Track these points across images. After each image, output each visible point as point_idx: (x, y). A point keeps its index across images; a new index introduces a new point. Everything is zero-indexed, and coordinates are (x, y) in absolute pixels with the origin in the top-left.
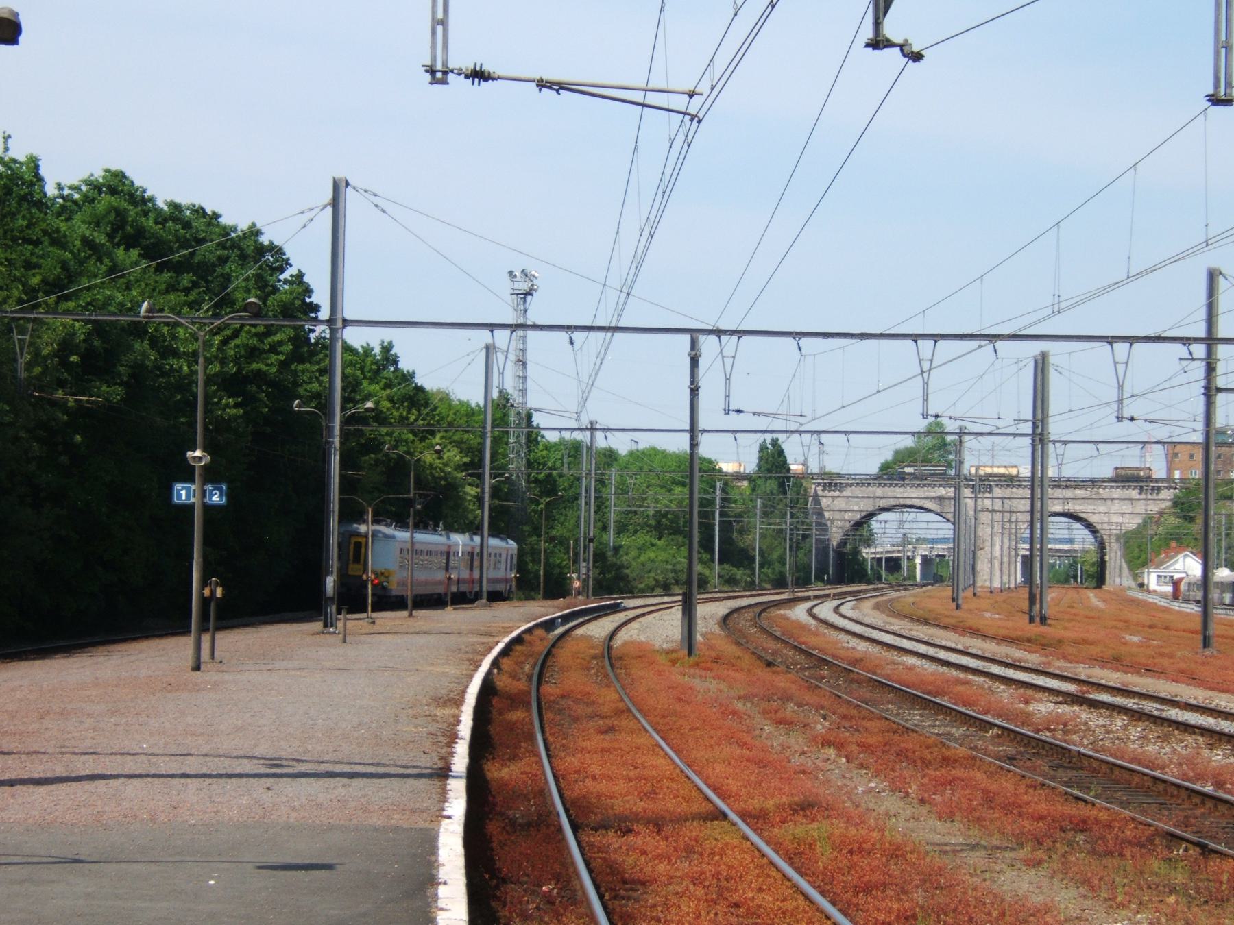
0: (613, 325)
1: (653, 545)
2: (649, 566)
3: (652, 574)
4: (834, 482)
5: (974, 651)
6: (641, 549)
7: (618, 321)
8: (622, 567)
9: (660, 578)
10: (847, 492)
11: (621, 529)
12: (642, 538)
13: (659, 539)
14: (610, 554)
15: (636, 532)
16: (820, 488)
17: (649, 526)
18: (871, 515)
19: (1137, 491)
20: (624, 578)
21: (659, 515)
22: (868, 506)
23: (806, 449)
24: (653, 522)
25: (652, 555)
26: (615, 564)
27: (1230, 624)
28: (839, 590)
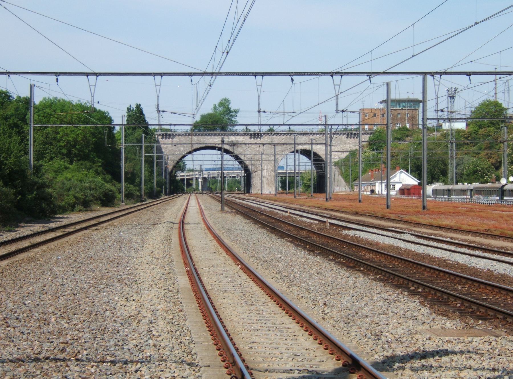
0: (217, 72)
1: (66, 168)
2: (68, 184)
3: (72, 192)
4: (168, 135)
5: (465, 227)
6: (58, 171)
7: (220, 70)
8: (44, 186)
9: (79, 195)
10: (176, 140)
11: (40, 155)
12: (58, 162)
13: (71, 163)
14: (30, 172)
15: (51, 159)
16: (160, 137)
17: (63, 154)
18: (184, 156)
19: (345, 136)
20: (48, 199)
21: (70, 146)
22: (184, 149)
23: (437, 87)
24: (64, 151)
25: (69, 176)
26: (36, 183)
27: (511, 201)
28: (242, 201)
